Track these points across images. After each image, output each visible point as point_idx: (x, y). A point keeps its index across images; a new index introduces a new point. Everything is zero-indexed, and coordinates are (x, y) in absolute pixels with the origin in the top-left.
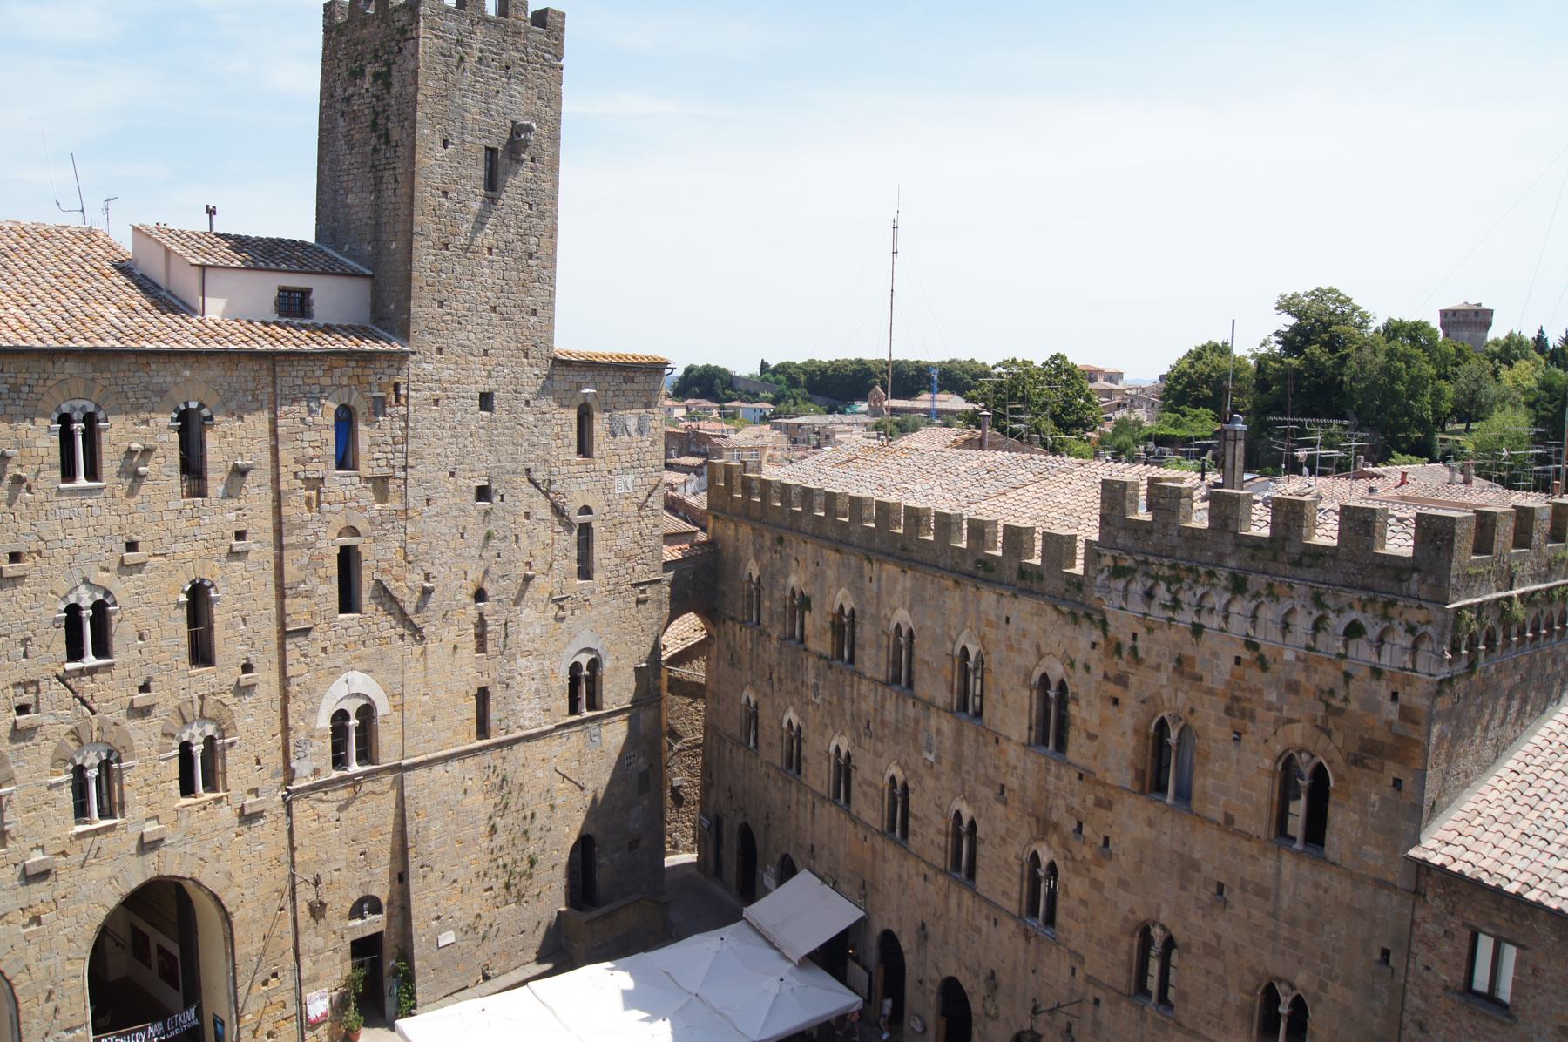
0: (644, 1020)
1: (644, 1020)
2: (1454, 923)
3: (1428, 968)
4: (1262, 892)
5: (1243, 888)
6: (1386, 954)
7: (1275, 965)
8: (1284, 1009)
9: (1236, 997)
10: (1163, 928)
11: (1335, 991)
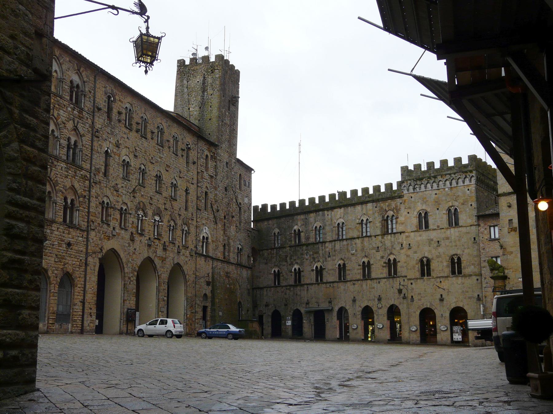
0: (471, 134)
1: (471, 134)
2: (486, 227)
3: (486, 297)
4: (448, 238)
5: (443, 240)
6: (475, 238)
7: (452, 252)
8: (456, 261)
9: (445, 264)
10: (426, 257)
11: (466, 251)
